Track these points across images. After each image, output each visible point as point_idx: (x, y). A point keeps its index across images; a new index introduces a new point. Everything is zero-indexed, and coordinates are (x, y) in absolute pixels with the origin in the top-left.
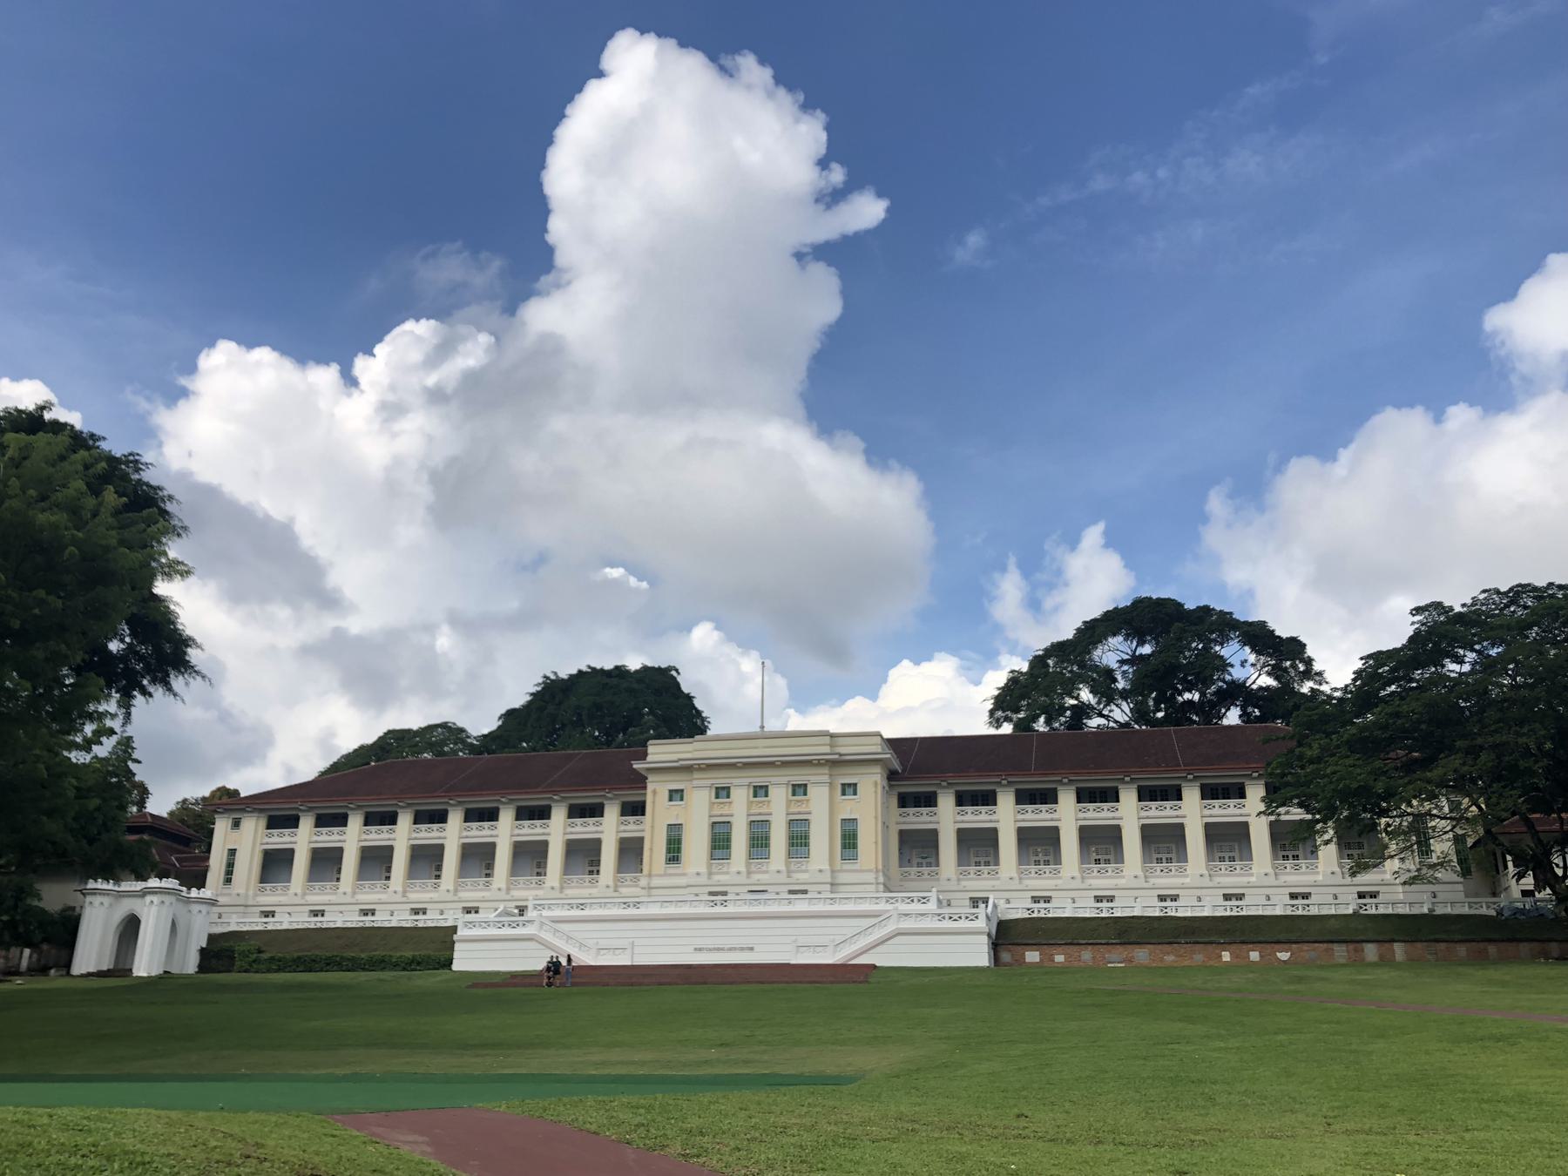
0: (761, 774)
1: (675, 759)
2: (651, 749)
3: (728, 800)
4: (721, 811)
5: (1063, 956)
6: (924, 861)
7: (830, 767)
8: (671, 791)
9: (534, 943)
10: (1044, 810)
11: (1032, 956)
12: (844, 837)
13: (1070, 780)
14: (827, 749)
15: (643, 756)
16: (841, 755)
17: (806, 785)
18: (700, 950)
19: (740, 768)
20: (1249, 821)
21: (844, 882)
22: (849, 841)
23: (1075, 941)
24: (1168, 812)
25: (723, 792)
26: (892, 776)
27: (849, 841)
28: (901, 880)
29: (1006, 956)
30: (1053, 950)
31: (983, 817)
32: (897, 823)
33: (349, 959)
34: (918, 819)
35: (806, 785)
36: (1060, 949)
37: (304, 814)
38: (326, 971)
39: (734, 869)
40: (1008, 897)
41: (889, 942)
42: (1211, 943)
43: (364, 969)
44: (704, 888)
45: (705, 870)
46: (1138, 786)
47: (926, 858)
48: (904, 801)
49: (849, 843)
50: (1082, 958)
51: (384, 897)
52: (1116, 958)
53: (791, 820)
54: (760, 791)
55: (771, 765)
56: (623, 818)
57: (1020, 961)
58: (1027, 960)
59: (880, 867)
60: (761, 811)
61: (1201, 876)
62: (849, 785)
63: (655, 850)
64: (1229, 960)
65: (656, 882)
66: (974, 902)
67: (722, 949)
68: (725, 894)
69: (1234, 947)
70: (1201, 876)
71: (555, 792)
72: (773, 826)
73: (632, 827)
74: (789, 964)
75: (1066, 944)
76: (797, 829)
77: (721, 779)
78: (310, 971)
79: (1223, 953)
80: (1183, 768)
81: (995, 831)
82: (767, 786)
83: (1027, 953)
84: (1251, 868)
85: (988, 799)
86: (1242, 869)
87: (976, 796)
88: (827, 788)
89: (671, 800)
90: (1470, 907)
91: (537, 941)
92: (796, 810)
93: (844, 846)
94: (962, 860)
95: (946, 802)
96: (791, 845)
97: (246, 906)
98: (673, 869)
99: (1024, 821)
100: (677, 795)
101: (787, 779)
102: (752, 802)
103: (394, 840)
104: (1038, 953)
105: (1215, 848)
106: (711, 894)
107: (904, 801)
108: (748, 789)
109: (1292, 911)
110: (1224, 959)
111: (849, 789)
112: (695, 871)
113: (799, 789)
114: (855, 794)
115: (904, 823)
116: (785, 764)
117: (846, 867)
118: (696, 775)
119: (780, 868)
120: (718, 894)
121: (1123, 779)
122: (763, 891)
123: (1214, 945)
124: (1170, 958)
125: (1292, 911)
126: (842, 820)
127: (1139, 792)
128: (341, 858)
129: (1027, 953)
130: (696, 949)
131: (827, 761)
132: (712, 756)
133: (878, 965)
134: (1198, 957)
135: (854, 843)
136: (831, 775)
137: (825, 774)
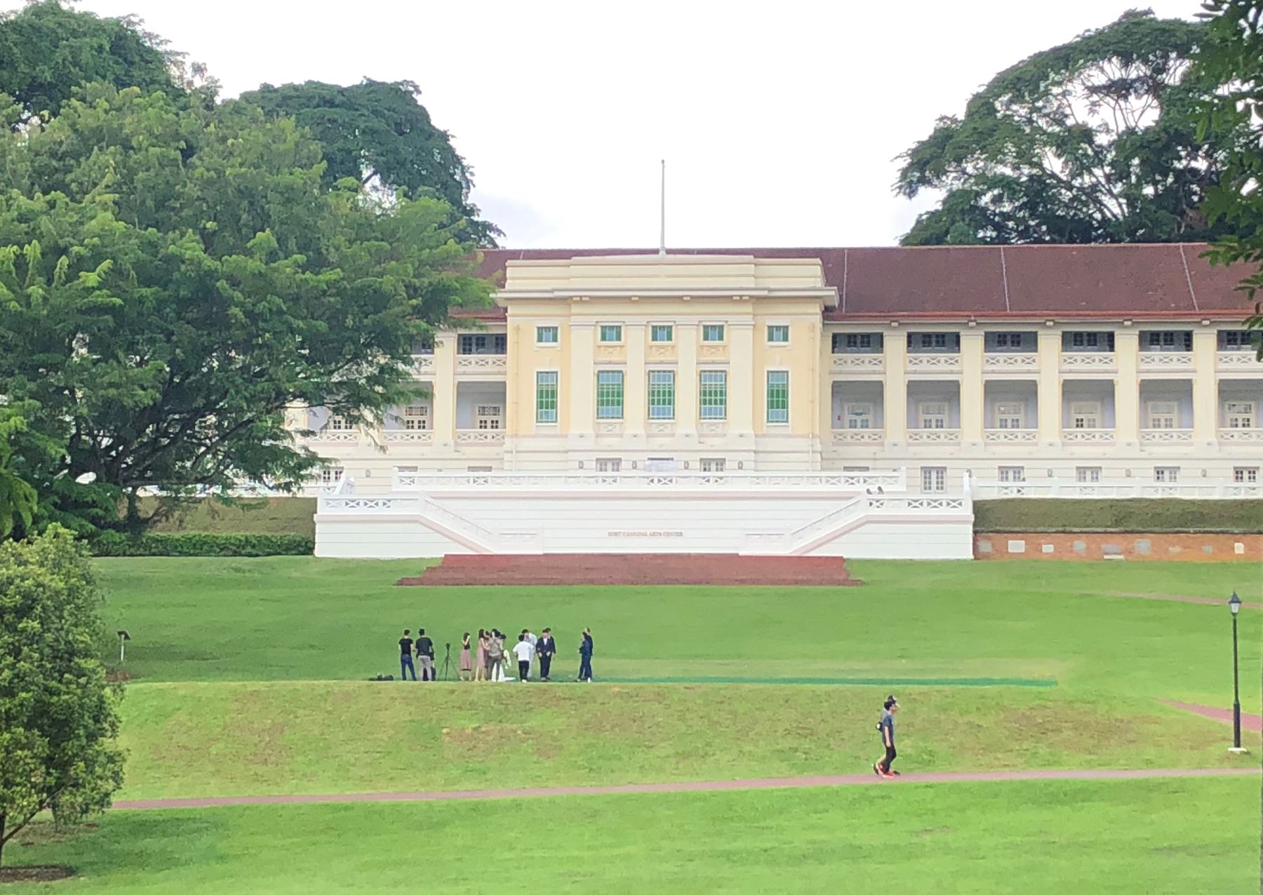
0: (592, 312)
1: (549, 288)
2: (510, 272)
3: (669, 343)
4: (611, 356)
5: (1052, 546)
6: (859, 419)
7: (754, 304)
8: (539, 328)
9: (419, 525)
10: (942, 360)
11: (1016, 546)
12: (771, 393)
13: (1133, 323)
14: (750, 283)
15: (501, 284)
16: (770, 290)
17: (721, 327)
18: (616, 534)
19: (586, 302)
20: (1115, 379)
21: (769, 449)
22: (778, 399)
23: (1068, 529)
24: (1175, 365)
25: (611, 333)
26: (828, 312)
27: (778, 399)
28: (834, 444)
29: (985, 547)
30: (1041, 539)
31: (942, 367)
32: (831, 373)
33: (158, 541)
34: (859, 367)
35: (721, 327)
36: (1049, 537)
37: (893, 333)
38: (132, 555)
39: (681, 430)
40: (1128, 467)
41: (858, 530)
42: (1223, 533)
43: (181, 554)
44: (694, 454)
45: (592, 432)
46: (1140, 332)
47: (861, 414)
48: (842, 342)
49: (547, 402)
50: (1074, 549)
51: (1110, 451)
52: (1113, 549)
53: (599, 372)
54: (661, 333)
55: (628, 299)
56: (1065, 353)
57: (1003, 551)
58: (1010, 550)
59: (817, 432)
60: (614, 359)
61: (1209, 444)
62: (778, 328)
63: (521, 399)
64: (1242, 552)
65: (526, 444)
66: (1237, 473)
67: (645, 535)
68: (415, 469)
69: (1249, 537)
70: (1209, 444)
71: (894, 318)
72: (679, 379)
73: (481, 367)
74: (737, 555)
75: (1057, 532)
76: (711, 384)
77: (611, 315)
78: (107, 555)
79: (1236, 544)
80: (1197, 311)
81: (1189, 383)
82: (670, 327)
83: (1010, 542)
84: (1190, 436)
85: (950, 342)
86: (1179, 437)
87: (1013, 342)
88: (750, 333)
89: (540, 340)
90: (1246, 493)
91: (421, 523)
92: (710, 359)
93: (771, 405)
94: (912, 422)
95: (972, 343)
96: (601, 403)
97: (875, 459)
98: (546, 428)
99: (993, 372)
100: (547, 334)
101: (648, 318)
102: (651, 347)
103: (1194, 371)
104: (1023, 542)
105: (1073, 408)
106: (471, 469)
107: (842, 342)
108: (698, 330)
109: (1006, 494)
110: (1237, 552)
111: (779, 333)
112: (578, 432)
113: (713, 332)
114: (555, 340)
115: (840, 373)
116: (593, 300)
117: (773, 431)
118: (575, 309)
119: (689, 432)
120: (609, 464)
121: (1045, 323)
122: (668, 459)
123: (1226, 535)
124: (1176, 550)
125: (1006, 494)
126: (769, 372)
127: (1063, 336)
128: (959, 392)
129: (1010, 542)
130: (610, 534)
131: (751, 297)
132: (517, 288)
133: (845, 557)
134: (1208, 548)
135: (783, 402)
136: (754, 315)
137: (748, 314)
